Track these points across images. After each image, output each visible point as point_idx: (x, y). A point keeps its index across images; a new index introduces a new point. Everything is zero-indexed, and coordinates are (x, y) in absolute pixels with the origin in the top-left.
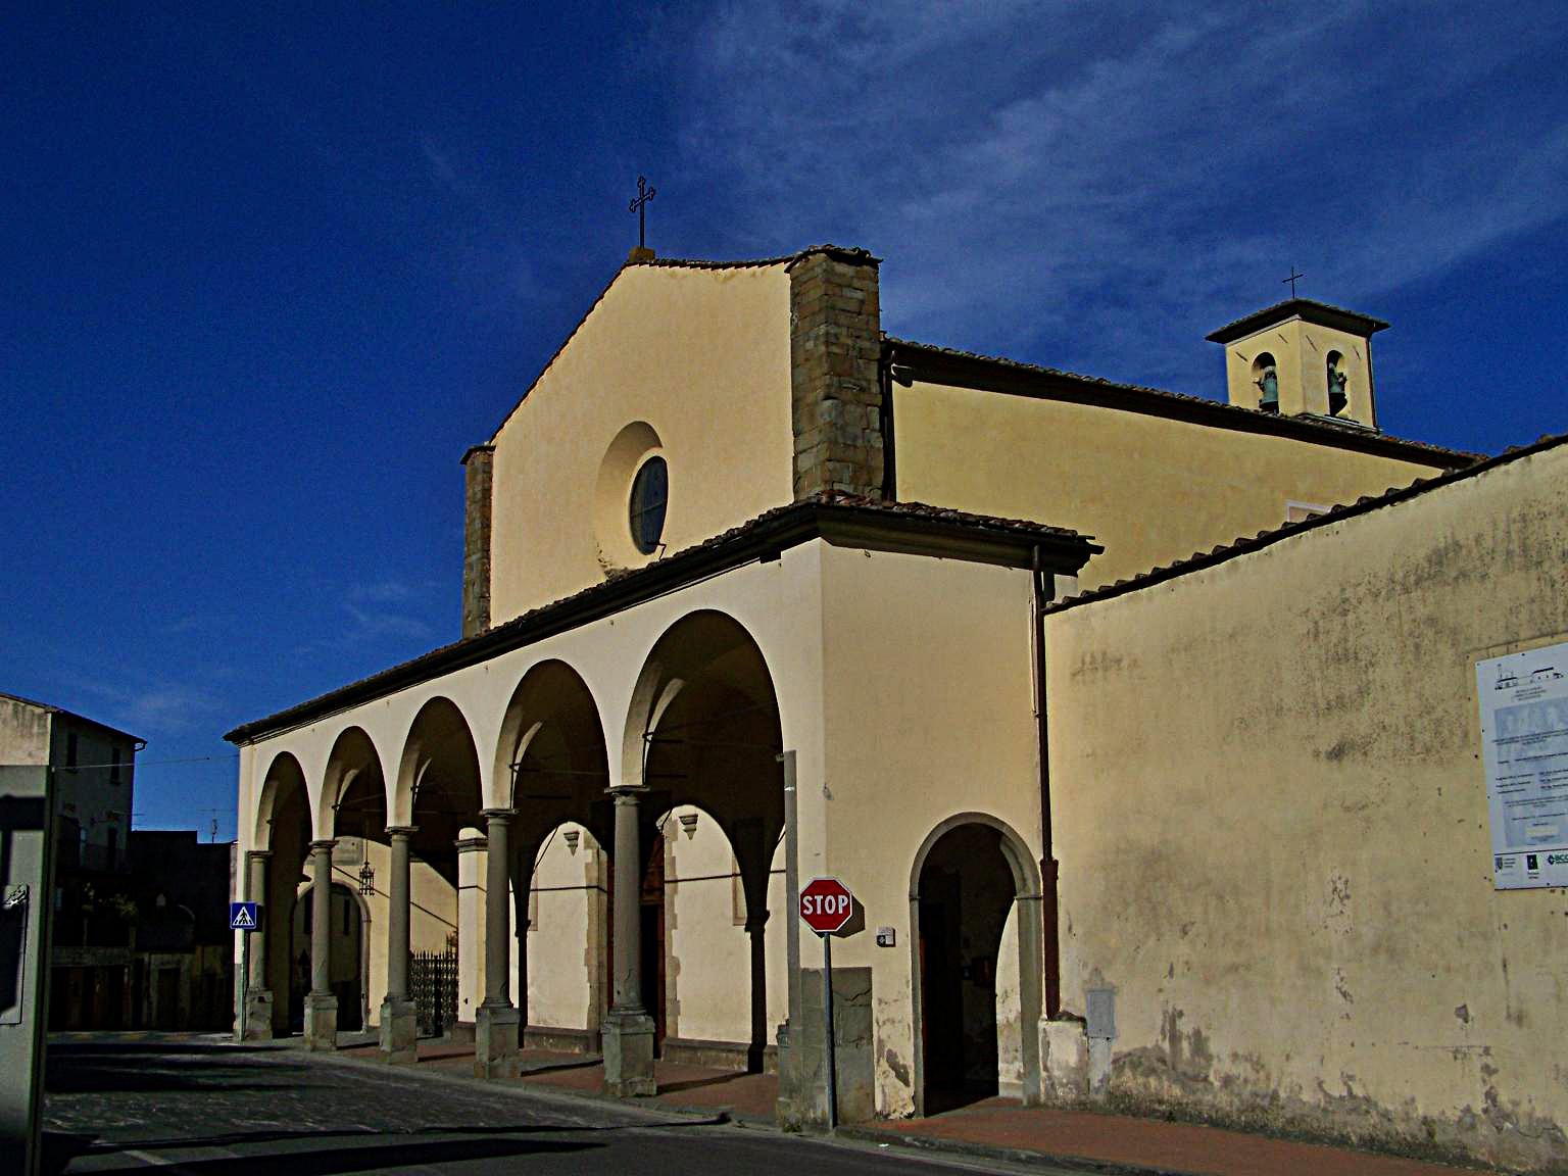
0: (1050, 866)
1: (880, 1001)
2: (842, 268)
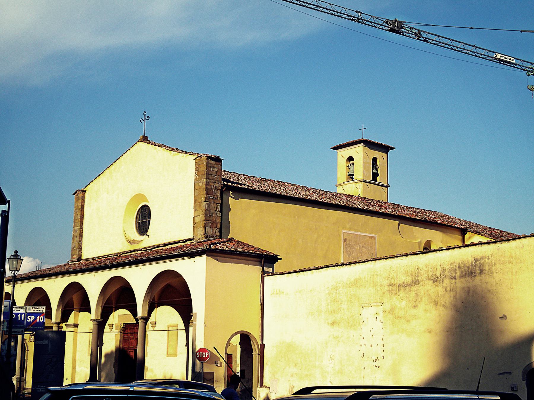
0: (263, 346)
2: (211, 162)
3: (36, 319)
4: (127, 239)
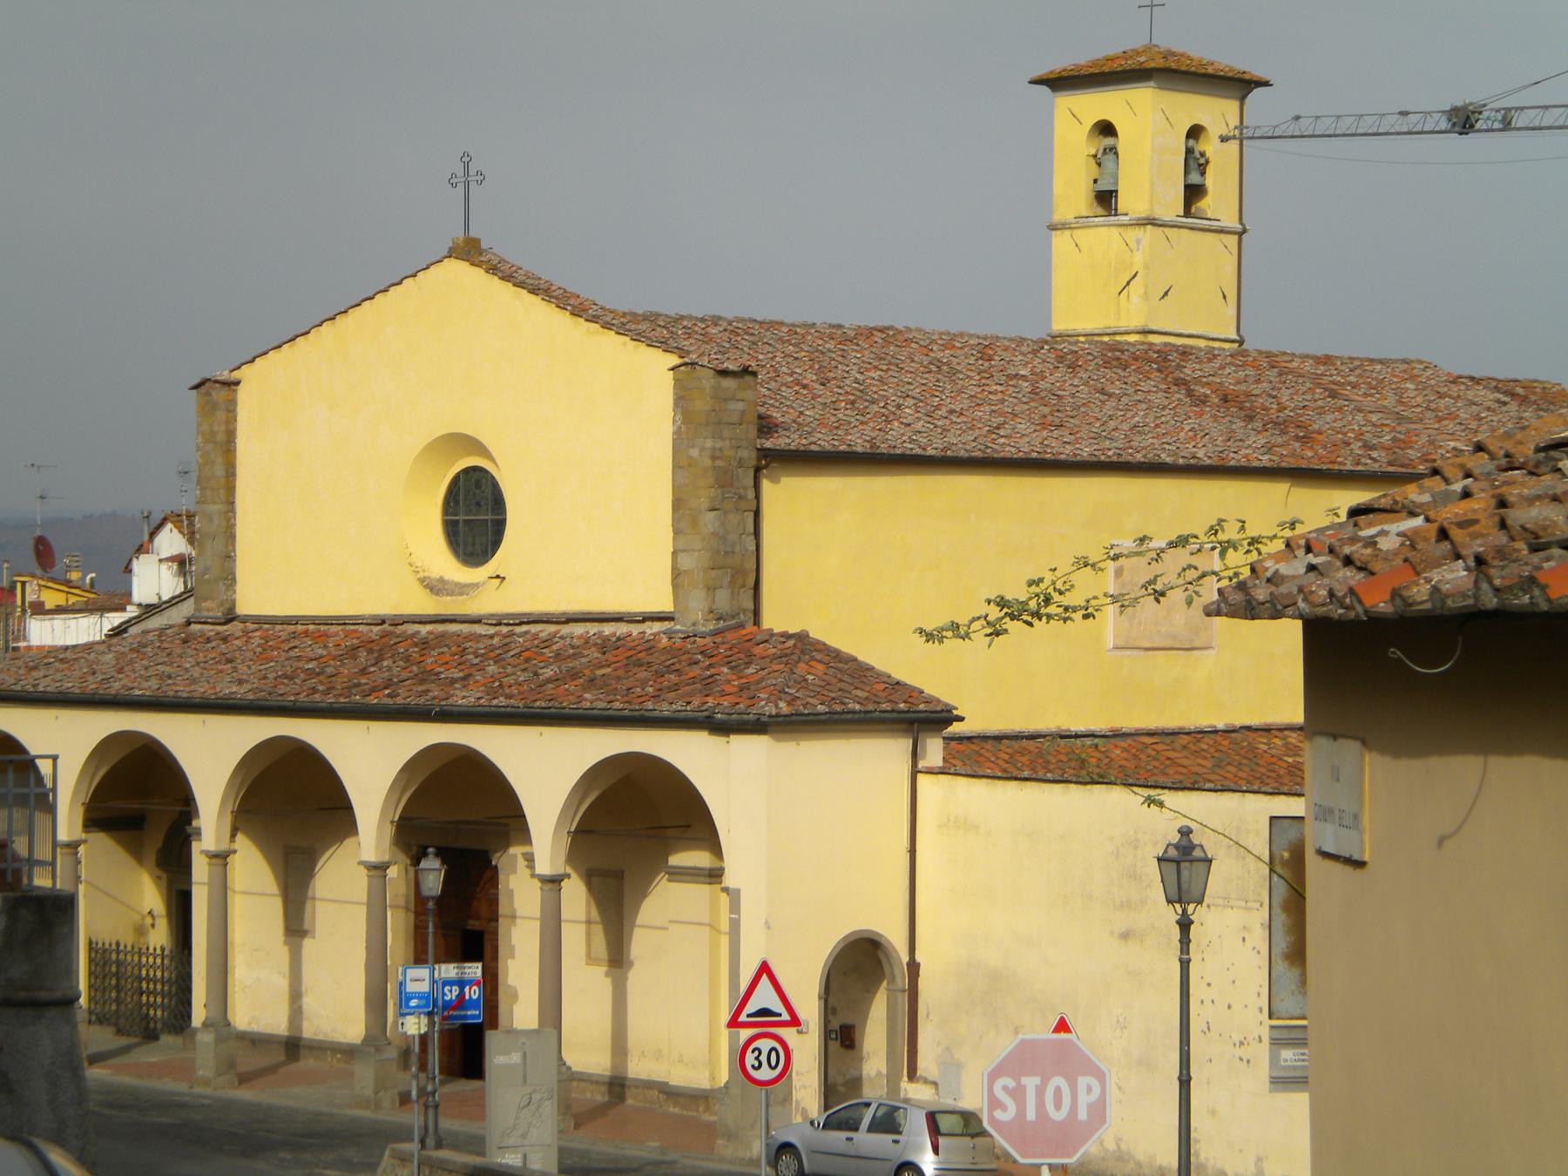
0: (914, 967)
1: (798, 1073)
2: (729, 383)
3: (462, 994)
4: (419, 576)
